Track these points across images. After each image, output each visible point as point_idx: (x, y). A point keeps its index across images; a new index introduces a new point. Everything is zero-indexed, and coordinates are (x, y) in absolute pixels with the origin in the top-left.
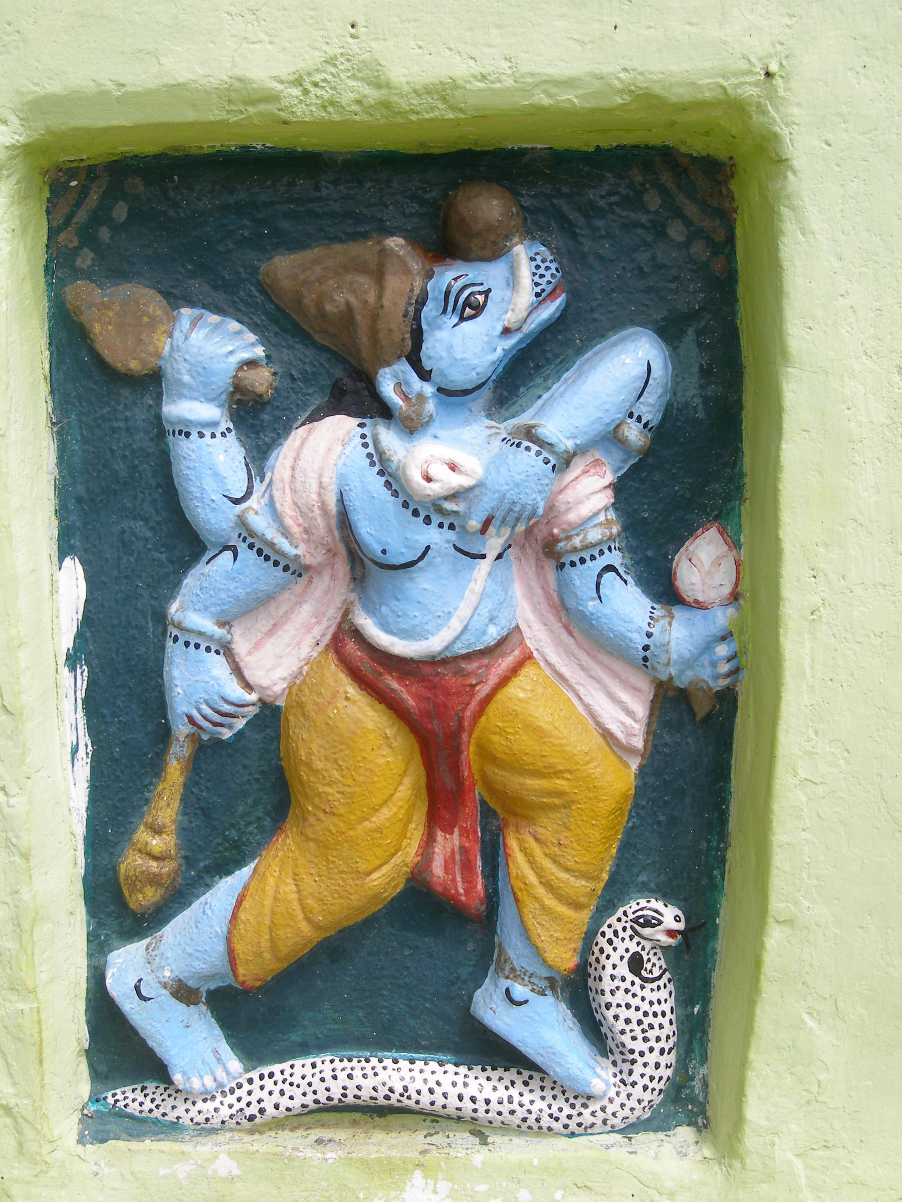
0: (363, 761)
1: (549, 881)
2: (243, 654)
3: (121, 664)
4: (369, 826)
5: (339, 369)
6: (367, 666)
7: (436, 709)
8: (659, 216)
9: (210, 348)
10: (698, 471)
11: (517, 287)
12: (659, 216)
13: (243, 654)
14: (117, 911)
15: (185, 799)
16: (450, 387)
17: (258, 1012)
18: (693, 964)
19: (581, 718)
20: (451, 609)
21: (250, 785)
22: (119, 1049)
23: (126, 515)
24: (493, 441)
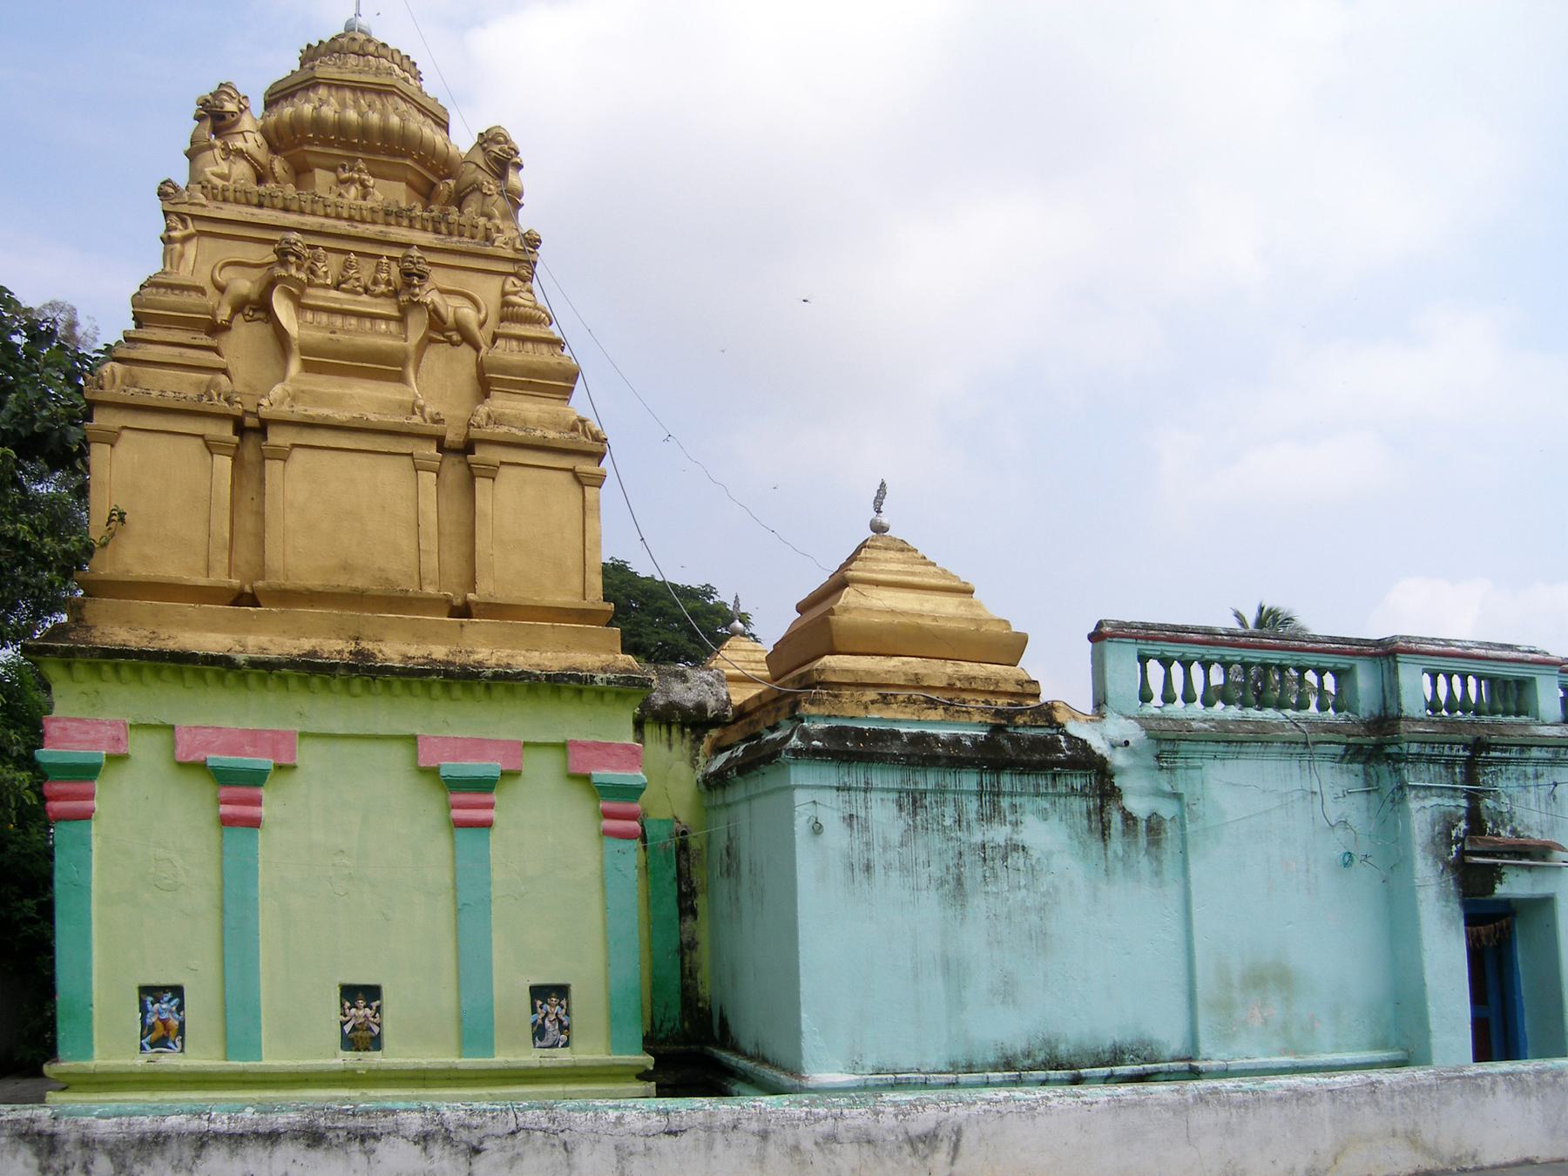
0: (160, 1025)
1: (172, 1034)
2: (151, 1019)
3: (143, 1019)
4: (160, 1031)
5: (157, 1000)
6: (879, 748)
7: (164, 1022)
8: (177, 991)
9: (150, 999)
10: (180, 1008)
11: (169, 995)
12: (177, 991)
13: (151, 1019)
14: (142, 1038)
15: (147, 1029)
16: (271, 345)
17: (152, 1045)
18: (183, 1041)
19: (174, 1023)
20: (164, 1016)
21: (152, 1028)
22: (142, 1048)
23: (144, 1009)
24: (166, 1006)
